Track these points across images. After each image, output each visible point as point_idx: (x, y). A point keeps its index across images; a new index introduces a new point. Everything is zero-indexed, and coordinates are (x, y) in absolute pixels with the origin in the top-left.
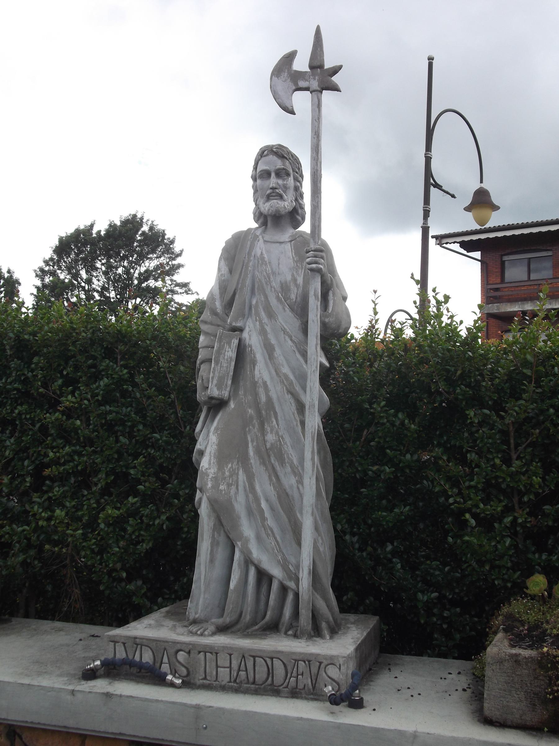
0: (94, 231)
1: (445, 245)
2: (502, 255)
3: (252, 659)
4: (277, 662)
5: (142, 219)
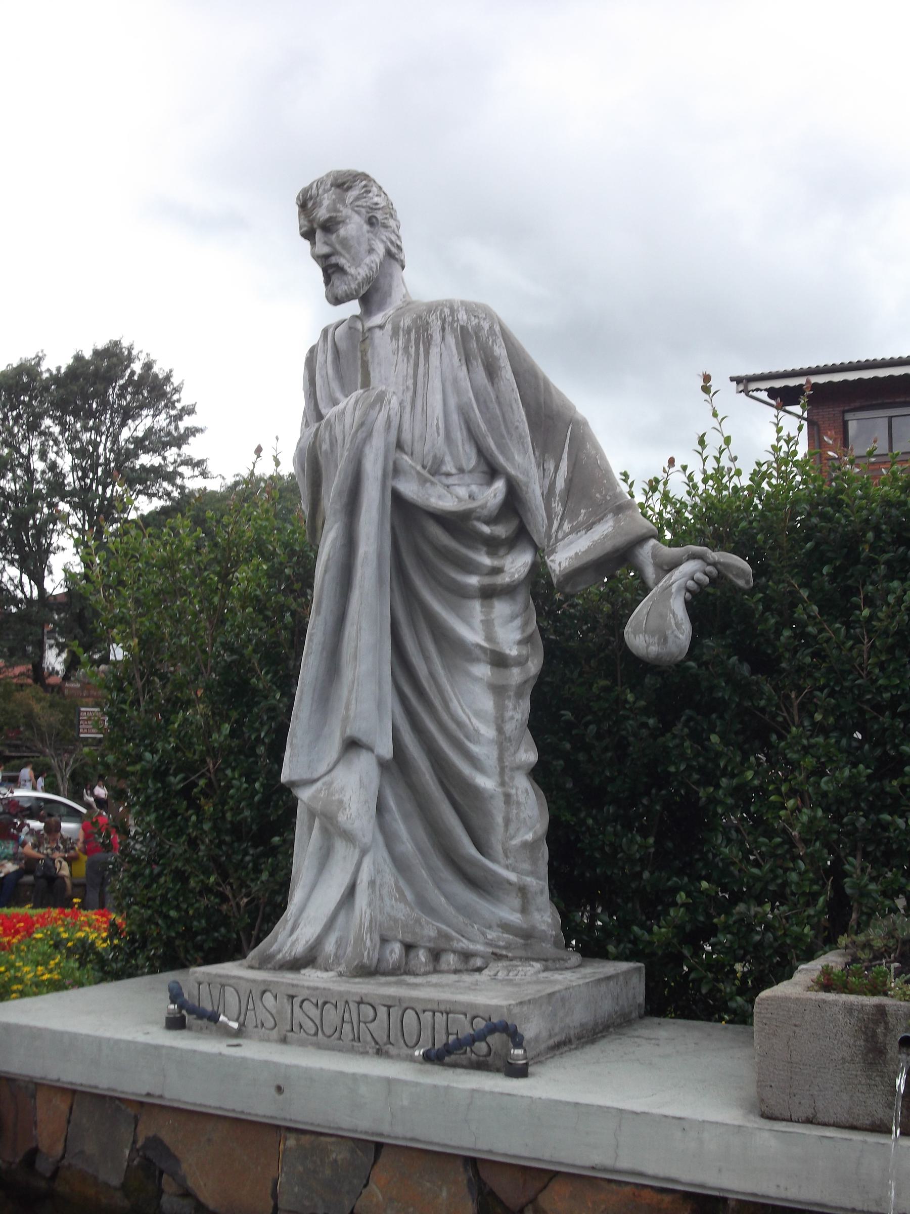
0: (44, 367)
1: (755, 394)
2: (844, 412)
3: (385, 1009)
4: (229, 991)
5: (130, 350)
